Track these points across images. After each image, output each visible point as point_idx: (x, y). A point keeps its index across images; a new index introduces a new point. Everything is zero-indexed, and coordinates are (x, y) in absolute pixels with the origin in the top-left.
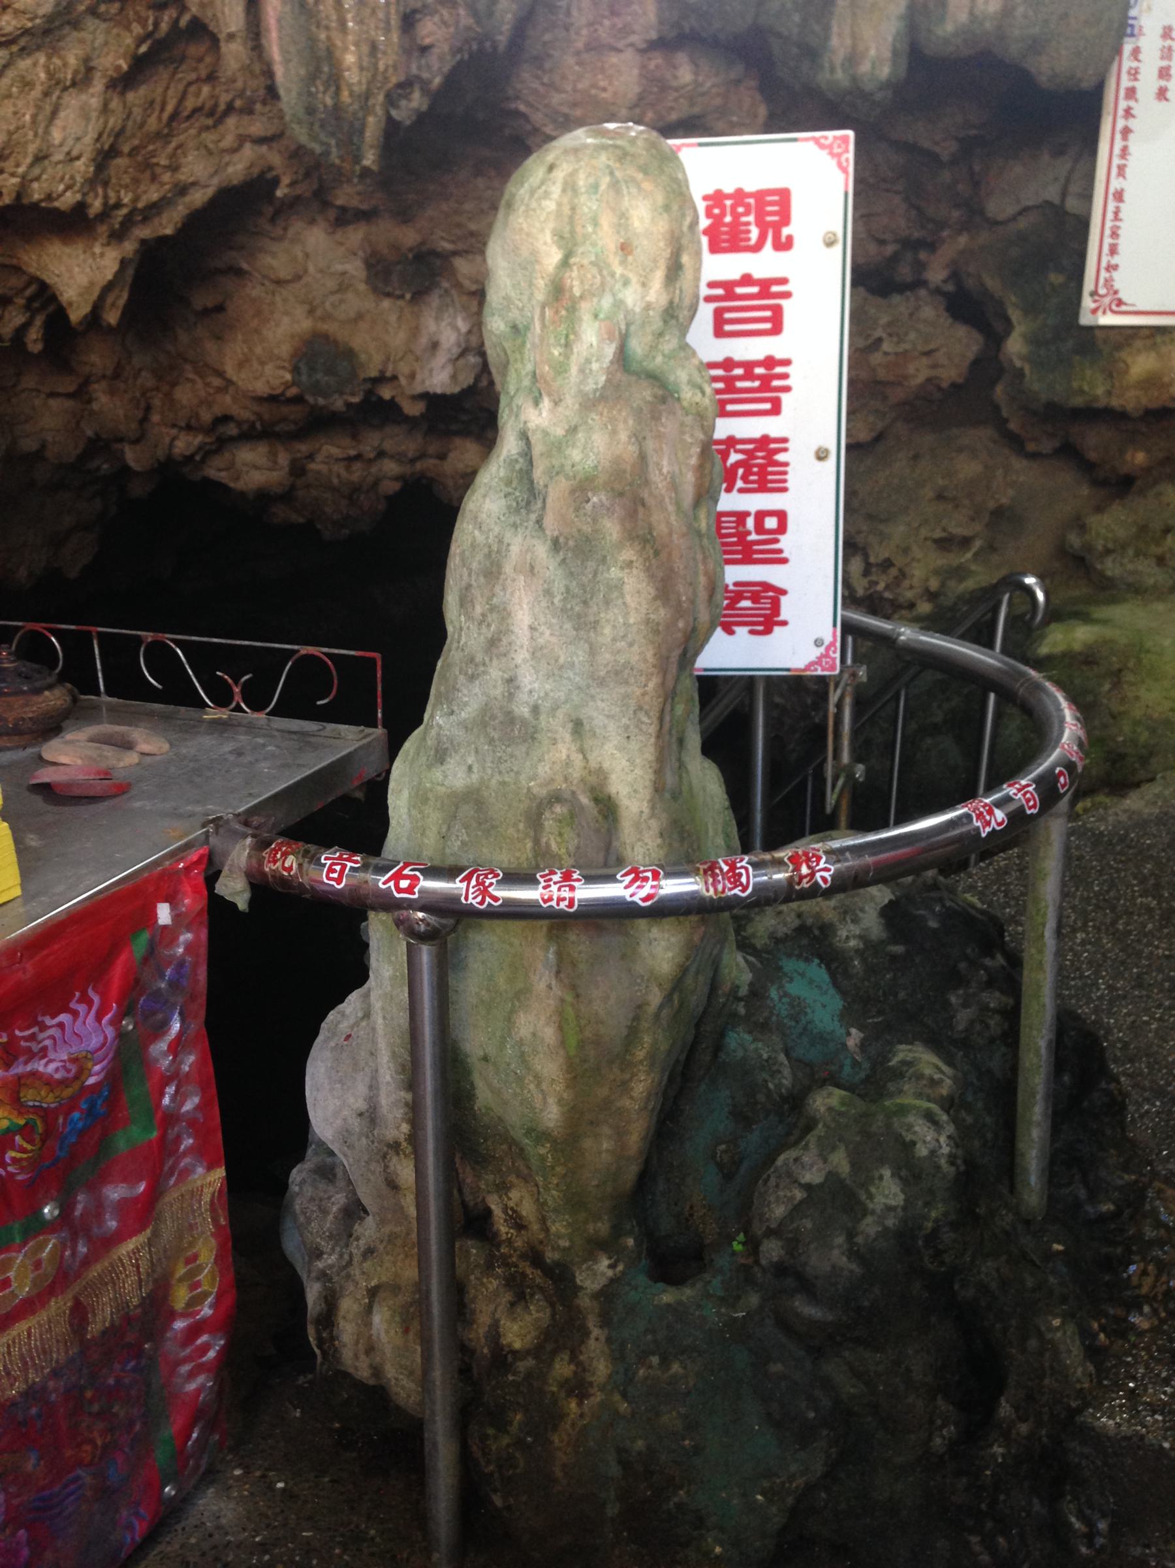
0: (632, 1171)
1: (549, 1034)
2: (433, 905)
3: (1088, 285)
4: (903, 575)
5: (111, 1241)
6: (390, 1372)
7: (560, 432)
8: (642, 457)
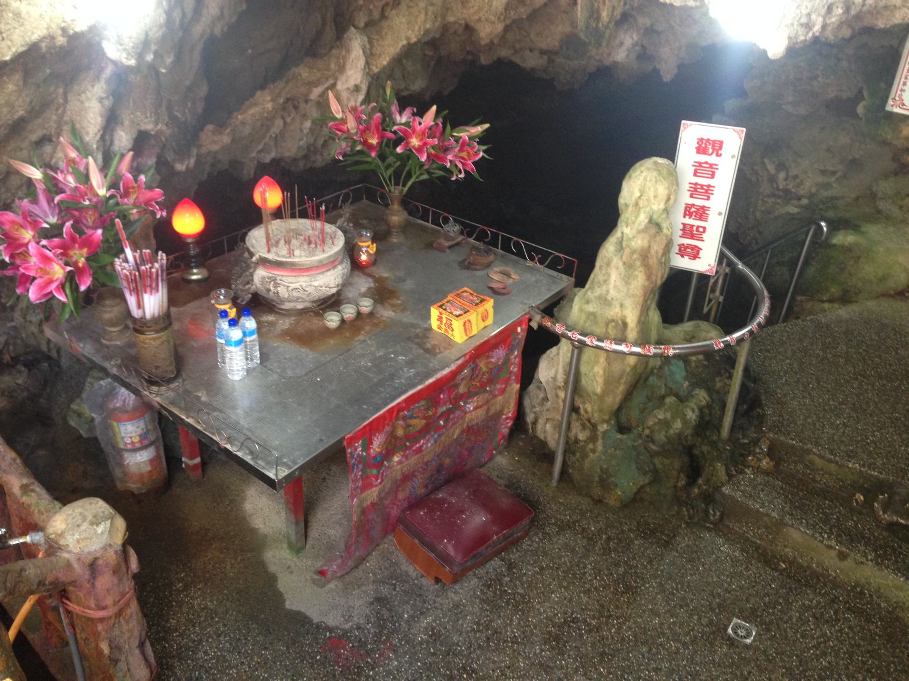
0: (616, 407)
1: (601, 372)
2: (580, 341)
3: (892, 95)
4: (802, 183)
5: (495, 396)
6: (549, 438)
7: (631, 236)
8: (650, 246)
